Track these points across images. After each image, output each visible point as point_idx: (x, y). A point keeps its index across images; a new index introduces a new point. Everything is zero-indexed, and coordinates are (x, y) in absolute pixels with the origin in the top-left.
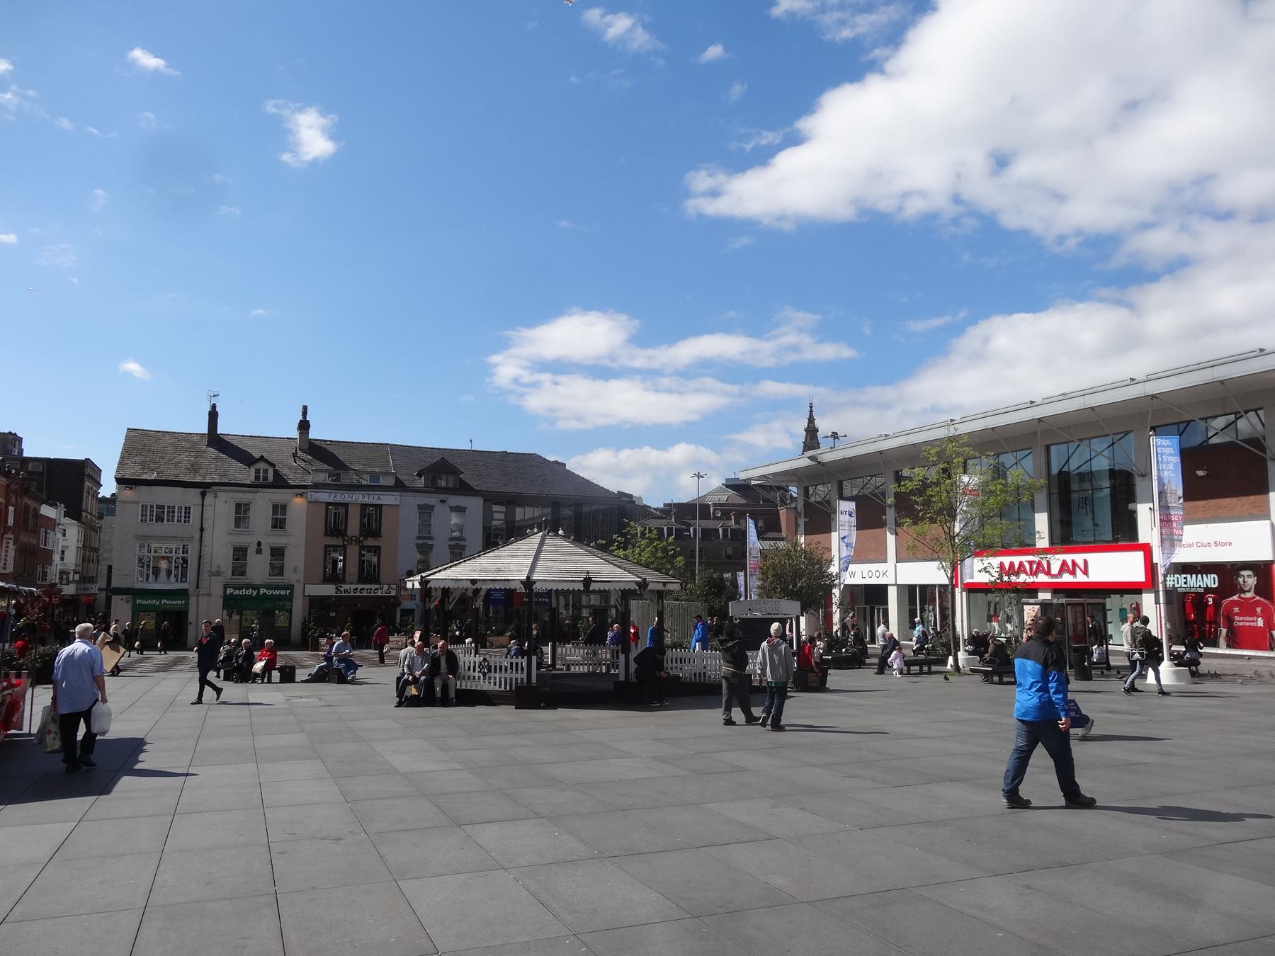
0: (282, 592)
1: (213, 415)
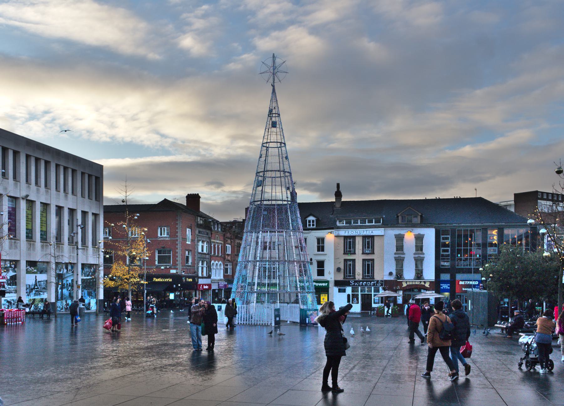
0: (324, 284)
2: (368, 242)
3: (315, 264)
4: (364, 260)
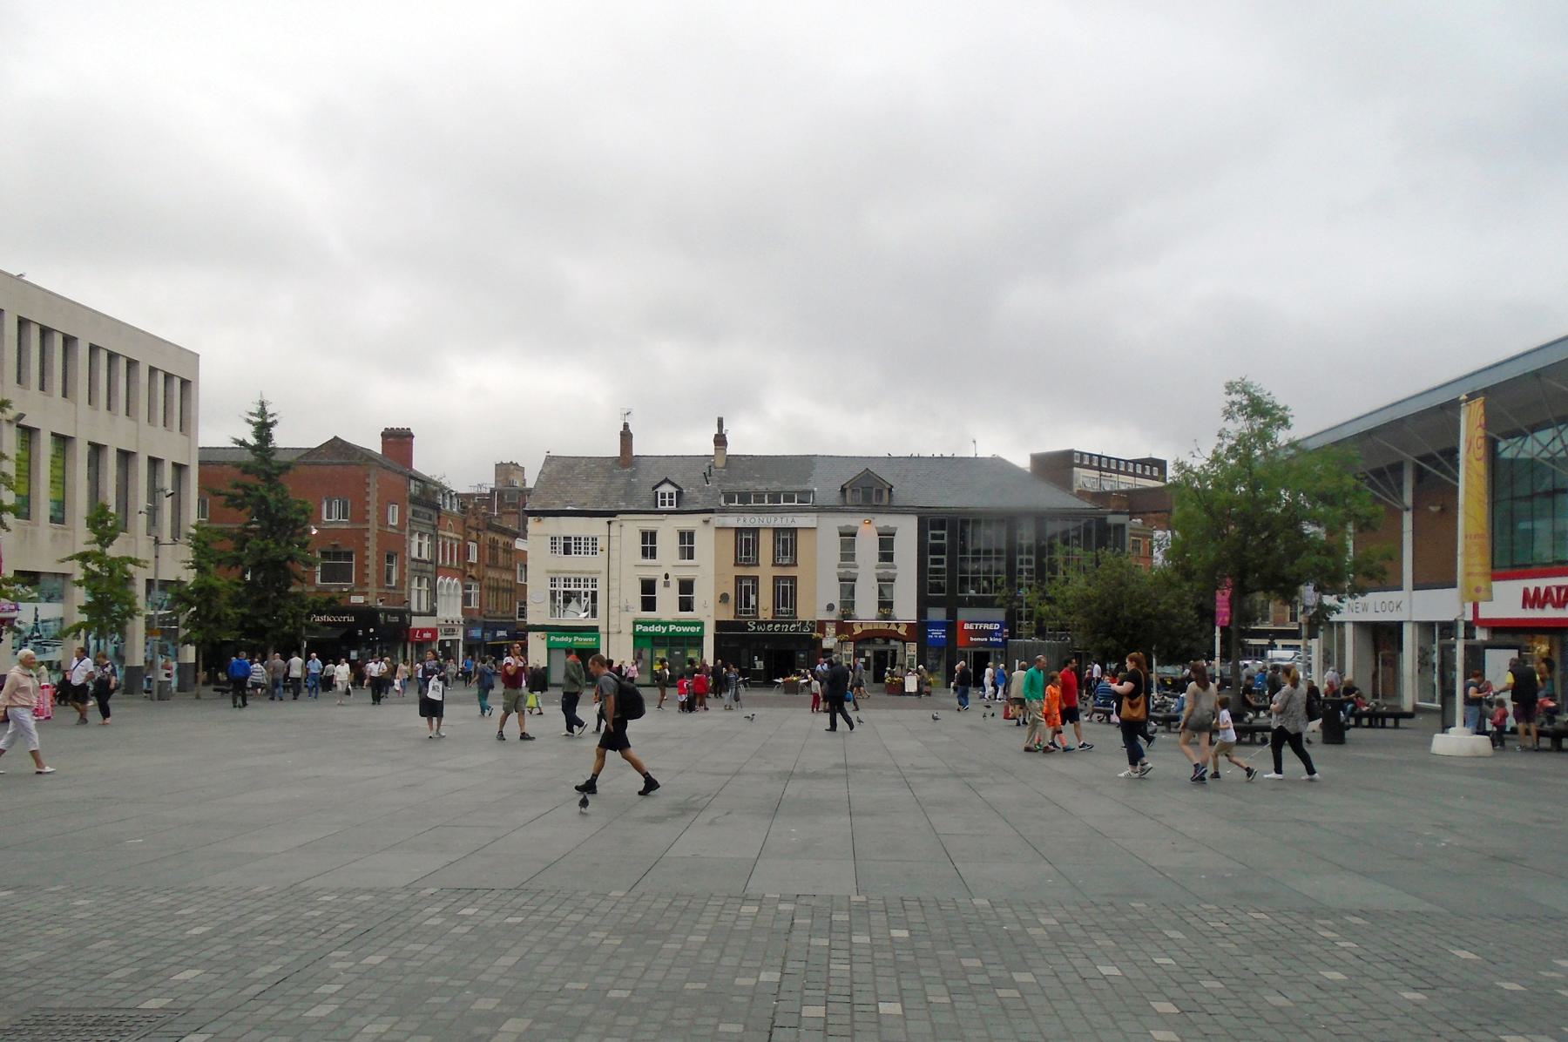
0: (693, 629)
1: (626, 436)
2: (785, 541)
3: (675, 586)
4: (776, 579)
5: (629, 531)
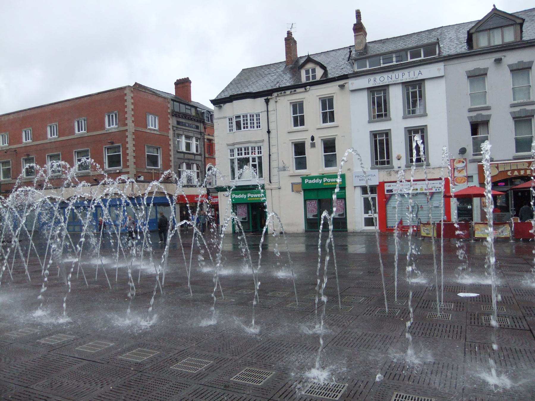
3: (320, 146)
5: (282, 106)
